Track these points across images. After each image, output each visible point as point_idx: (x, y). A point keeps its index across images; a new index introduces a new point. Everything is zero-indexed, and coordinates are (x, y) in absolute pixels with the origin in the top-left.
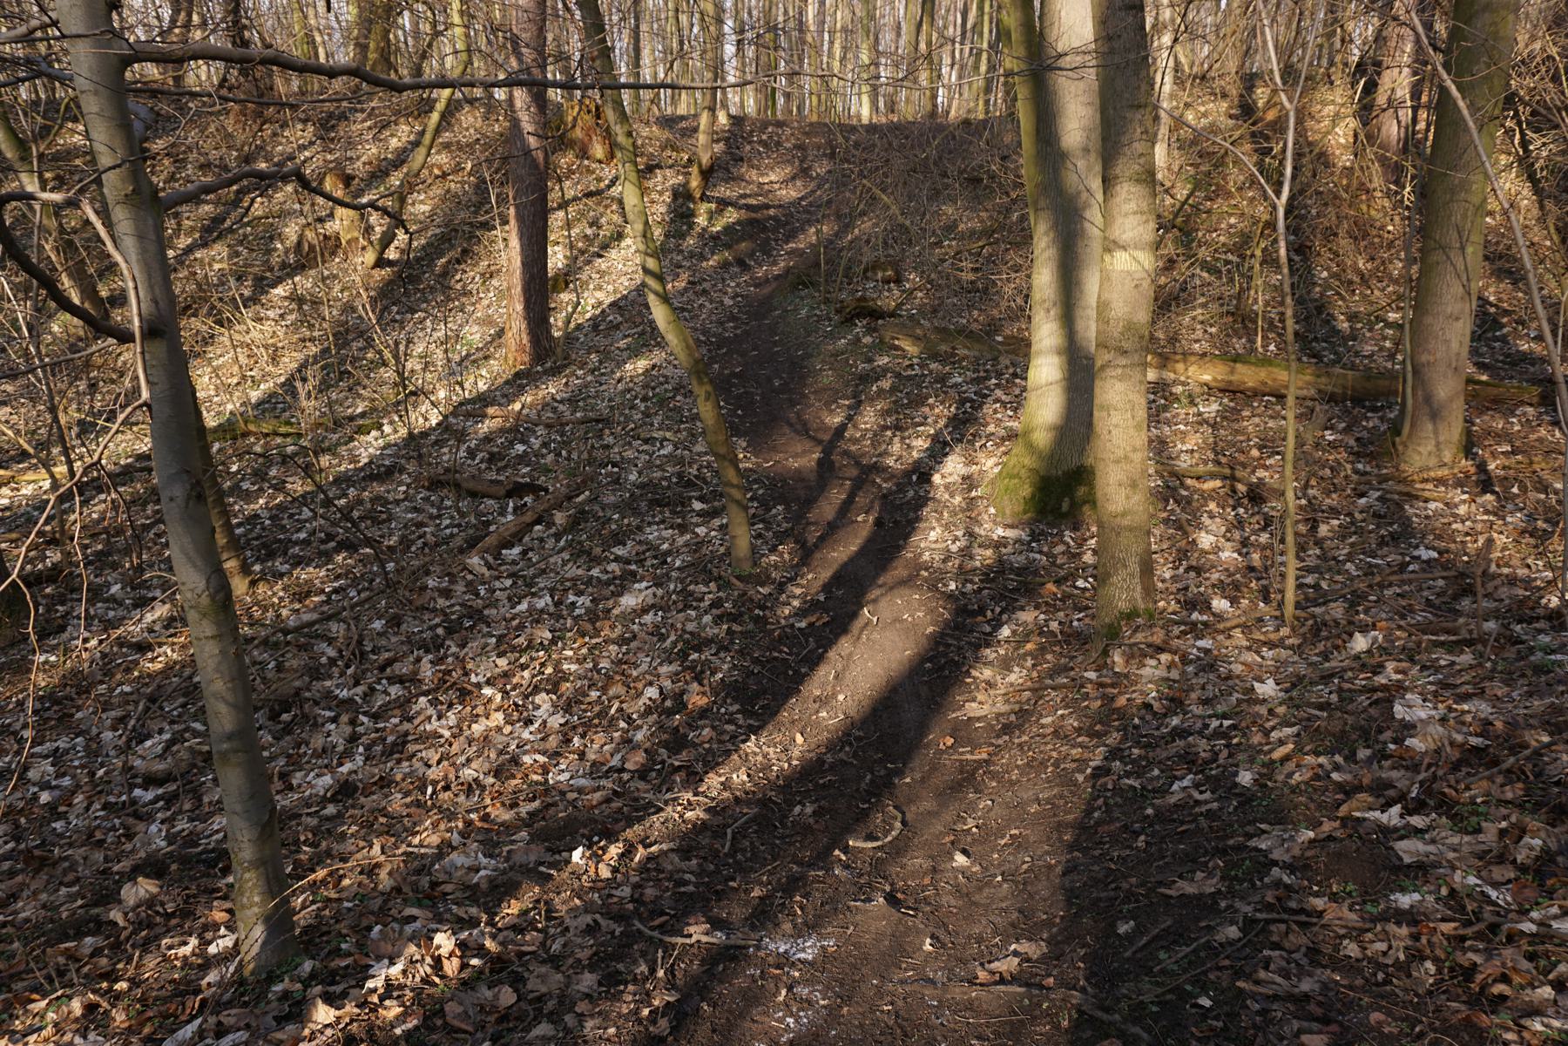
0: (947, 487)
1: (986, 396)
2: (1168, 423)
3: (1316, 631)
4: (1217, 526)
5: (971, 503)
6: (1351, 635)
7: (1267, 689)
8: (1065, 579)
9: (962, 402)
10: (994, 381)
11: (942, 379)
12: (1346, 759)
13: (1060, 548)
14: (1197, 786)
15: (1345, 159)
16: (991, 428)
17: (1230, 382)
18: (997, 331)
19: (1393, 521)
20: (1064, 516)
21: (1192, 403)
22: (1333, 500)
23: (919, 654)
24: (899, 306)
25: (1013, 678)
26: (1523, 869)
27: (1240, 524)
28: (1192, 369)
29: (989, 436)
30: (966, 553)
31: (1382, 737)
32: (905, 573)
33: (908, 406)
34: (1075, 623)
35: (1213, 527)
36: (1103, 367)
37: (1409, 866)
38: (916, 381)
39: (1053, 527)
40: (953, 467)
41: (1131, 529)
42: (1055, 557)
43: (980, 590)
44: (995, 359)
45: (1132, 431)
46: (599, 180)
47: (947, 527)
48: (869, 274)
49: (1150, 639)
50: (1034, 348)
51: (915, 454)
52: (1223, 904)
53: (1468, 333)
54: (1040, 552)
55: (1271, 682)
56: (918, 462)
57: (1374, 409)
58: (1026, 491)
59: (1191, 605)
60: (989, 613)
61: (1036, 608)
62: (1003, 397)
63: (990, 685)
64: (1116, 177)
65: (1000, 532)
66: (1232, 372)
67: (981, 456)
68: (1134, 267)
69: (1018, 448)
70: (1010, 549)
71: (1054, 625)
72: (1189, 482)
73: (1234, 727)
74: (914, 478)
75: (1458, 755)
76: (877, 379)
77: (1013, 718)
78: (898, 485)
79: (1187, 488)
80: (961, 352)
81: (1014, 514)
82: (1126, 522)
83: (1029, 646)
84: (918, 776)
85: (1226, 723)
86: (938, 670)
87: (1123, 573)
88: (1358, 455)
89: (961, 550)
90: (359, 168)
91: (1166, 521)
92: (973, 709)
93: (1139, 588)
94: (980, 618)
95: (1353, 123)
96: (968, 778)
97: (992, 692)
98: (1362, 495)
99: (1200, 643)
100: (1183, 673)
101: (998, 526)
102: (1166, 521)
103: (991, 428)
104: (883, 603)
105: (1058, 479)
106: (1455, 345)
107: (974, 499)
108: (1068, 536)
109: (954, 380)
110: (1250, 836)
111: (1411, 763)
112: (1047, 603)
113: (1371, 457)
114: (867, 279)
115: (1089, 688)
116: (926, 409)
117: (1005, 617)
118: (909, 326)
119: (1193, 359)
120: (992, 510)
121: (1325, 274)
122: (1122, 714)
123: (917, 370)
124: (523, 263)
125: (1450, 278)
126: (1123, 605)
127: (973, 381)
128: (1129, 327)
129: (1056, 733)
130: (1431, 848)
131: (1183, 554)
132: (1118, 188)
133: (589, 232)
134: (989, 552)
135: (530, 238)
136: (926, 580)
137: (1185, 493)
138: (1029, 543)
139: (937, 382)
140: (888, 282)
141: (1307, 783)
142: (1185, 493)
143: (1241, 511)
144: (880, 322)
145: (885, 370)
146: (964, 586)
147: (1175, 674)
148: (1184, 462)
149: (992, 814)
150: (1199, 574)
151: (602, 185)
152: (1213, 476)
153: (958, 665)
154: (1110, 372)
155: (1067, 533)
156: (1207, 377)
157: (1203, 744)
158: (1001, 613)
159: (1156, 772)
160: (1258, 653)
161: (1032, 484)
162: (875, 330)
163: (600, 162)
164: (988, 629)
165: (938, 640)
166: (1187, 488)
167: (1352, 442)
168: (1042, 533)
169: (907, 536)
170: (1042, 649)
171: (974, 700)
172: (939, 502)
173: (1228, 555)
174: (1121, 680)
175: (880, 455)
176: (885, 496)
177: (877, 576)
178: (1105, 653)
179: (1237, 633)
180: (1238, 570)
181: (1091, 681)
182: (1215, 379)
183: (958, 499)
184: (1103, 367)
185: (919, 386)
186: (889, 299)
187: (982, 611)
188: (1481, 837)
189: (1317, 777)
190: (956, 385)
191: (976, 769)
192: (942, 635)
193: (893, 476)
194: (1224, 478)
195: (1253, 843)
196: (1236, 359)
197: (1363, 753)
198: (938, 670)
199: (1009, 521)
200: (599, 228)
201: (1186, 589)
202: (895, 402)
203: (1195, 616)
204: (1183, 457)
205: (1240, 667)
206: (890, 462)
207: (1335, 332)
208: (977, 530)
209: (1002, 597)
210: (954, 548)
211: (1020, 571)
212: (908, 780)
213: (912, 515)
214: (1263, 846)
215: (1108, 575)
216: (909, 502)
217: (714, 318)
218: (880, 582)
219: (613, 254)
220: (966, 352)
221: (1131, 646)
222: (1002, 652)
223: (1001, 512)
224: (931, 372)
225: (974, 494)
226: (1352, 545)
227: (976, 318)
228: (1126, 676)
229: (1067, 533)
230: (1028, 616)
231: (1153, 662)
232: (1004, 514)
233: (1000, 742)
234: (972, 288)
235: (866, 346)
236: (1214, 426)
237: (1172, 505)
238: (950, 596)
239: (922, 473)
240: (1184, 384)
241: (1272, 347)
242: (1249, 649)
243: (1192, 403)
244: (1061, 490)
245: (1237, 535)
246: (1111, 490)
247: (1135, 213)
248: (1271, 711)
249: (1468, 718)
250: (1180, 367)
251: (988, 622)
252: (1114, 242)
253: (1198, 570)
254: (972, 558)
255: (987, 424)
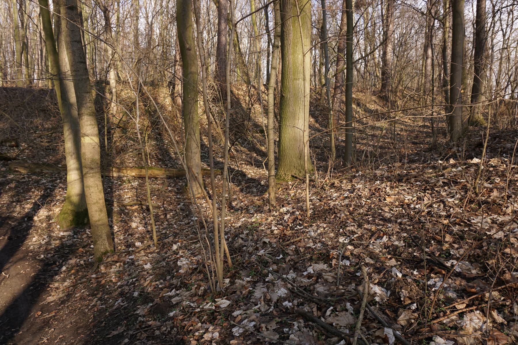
0: (40, 221)
1: (56, 186)
2: (122, 189)
3: (163, 246)
4: (137, 220)
5: (50, 225)
6: (172, 245)
7: (148, 266)
8: (87, 246)
9: (46, 189)
10: (58, 181)
11: (37, 182)
12: (164, 281)
13: (85, 236)
14: (122, 301)
15: (170, 108)
16: (58, 198)
17: (141, 175)
18: (59, 163)
19: (187, 211)
20: (86, 224)
21: (130, 182)
22: (171, 207)
23: (28, 284)
24: (18, 155)
25: (66, 284)
26: (200, 296)
27: (144, 218)
28: (129, 172)
29: (57, 201)
30: (48, 243)
31: (173, 272)
32: (22, 256)
33: (23, 192)
34: (90, 260)
35: (136, 221)
36: (85, 174)
37: (175, 304)
38: (27, 183)
39: (82, 229)
40: (43, 213)
41: (102, 225)
42: (83, 239)
43: (54, 256)
44: (59, 173)
45: (98, 194)
47: (40, 235)
48: (4, 144)
49: (113, 259)
50: (68, 169)
51: (26, 210)
52: (125, 334)
53: (199, 157)
54: (78, 238)
55: (149, 264)
56: (28, 213)
57: (181, 180)
58: (71, 218)
59: (128, 246)
60: (58, 263)
61: (76, 258)
62: (63, 186)
63: (57, 288)
64: (82, 114)
65: (62, 234)
66: (141, 172)
67: (54, 208)
68: (92, 142)
69: (66, 203)
70: (66, 239)
71: (82, 262)
72: (128, 207)
73: (137, 280)
74: (26, 219)
75: (191, 271)
76: (9, 184)
77: (65, 298)
78: (18, 223)
79: (127, 210)
80: (45, 171)
81: (67, 227)
82: (100, 223)
83: (73, 271)
84: (25, 330)
85: (134, 280)
86: (36, 288)
87: (101, 240)
88: (177, 193)
89: (46, 243)
91: (121, 221)
92: (50, 299)
93: (107, 243)
94: (54, 266)
95: (170, 98)
96: (47, 323)
97: (57, 291)
98: (179, 204)
99: (130, 257)
100: (124, 267)
101: (60, 232)
102: (121, 221)
103: (58, 198)
104: (12, 269)
105: (82, 212)
106: (197, 160)
107: (50, 224)
108: (88, 231)
109: (42, 182)
110: (135, 311)
111: (179, 276)
112: (80, 255)
113: (181, 193)
114: (3, 146)
115: (93, 281)
116: (31, 193)
117: (64, 263)
118: (23, 163)
119: (128, 168)
120: (58, 226)
121: (167, 141)
122: (104, 286)
123: (27, 179)
125: (193, 142)
126: (103, 250)
127: (50, 181)
128: (93, 161)
129: (81, 299)
130: (180, 298)
131: (126, 231)
132: (83, 117)
134: (58, 242)
136: (31, 256)
137: (127, 211)
138: (73, 236)
139: (35, 183)
140: (13, 147)
141: (152, 291)
142: (127, 211)
143: (145, 214)
144: (9, 162)
145: (12, 180)
146: (47, 255)
147: (121, 269)
148: (127, 202)
149: (54, 333)
150: (132, 236)
152: (135, 205)
153: (44, 285)
154: (88, 175)
155: (87, 230)
156: (134, 174)
157: (127, 288)
158: (62, 262)
159: (111, 301)
160: (147, 256)
161: (73, 215)
162: (7, 165)
164: (57, 269)
165: (36, 278)
166: (127, 210)
167: (176, 190)
168: (78, 232)
169: (24, 241)
170: (78, 271)
171: (50, 295)
172: (37, 226)
173: (141, 228)
174: (104, 275)
175: (10, 212)
176: (13, 228)
177: (9, 259)
178: (98, 267)
179: (142, 252)
180: (144, 232)
181: (93, 278)
182: (136, 174)
183: (44, 224)
184: (85, 174)
185: (27, 185)
186: (13, 153)
187: (55, 263)
188: (192, 291)
189: (155, 288)
190: (43, 183)
191: (50, 320)
192: (37, 275)
193: (16, 220)
194: (139, 205)
195: (135, 313)
196: (142, 168)
197: (168, 278)
198: (36, 288)
199: (65, 229)
201: (128, 241)
202: (17, 192)
203: (131, 249)
204: (127, 200)
205: (142, 262)
206: (15, 214)
207: (171, 158)
208: (52, 234)
209: (63, 256)
210: (43, 243)
211: (70, 246)
212: (21, 333)
213: (25, 233)
214: (138, 312)
215: (96, 241)
216: (24, 229)
218: (10, 261)
220: (47, 171)
221: (106, 263)
222: (62, 276)
223: (62, 227)
224: (33, 180)
225: (51, 222)
226: (176, 219)
227: (51, 159)
228: (105, 273)
229: (87, 230)
230: (73, 261)
231: (115, 267)
232: (63, 227)
233: (60, 307)
234: (47, 149)
235: (3, 171)
236: (137, 189)
237: (123, 215)
238: (42, 260)
239: (29, 217)
240: (126, 177)
241: (154, 163)
242: (145, 256)
243: (130, 182)
244: (80, 217)
245: (143, 222)
246: (93, 213)
247: (90, 125)
248: (148, 273)
249: (194, 261)
250: (125, 171)
251: (57, 267)
252: (84, 134)
253: (132, 235)
254: (51, 245)
255: (57, 196)
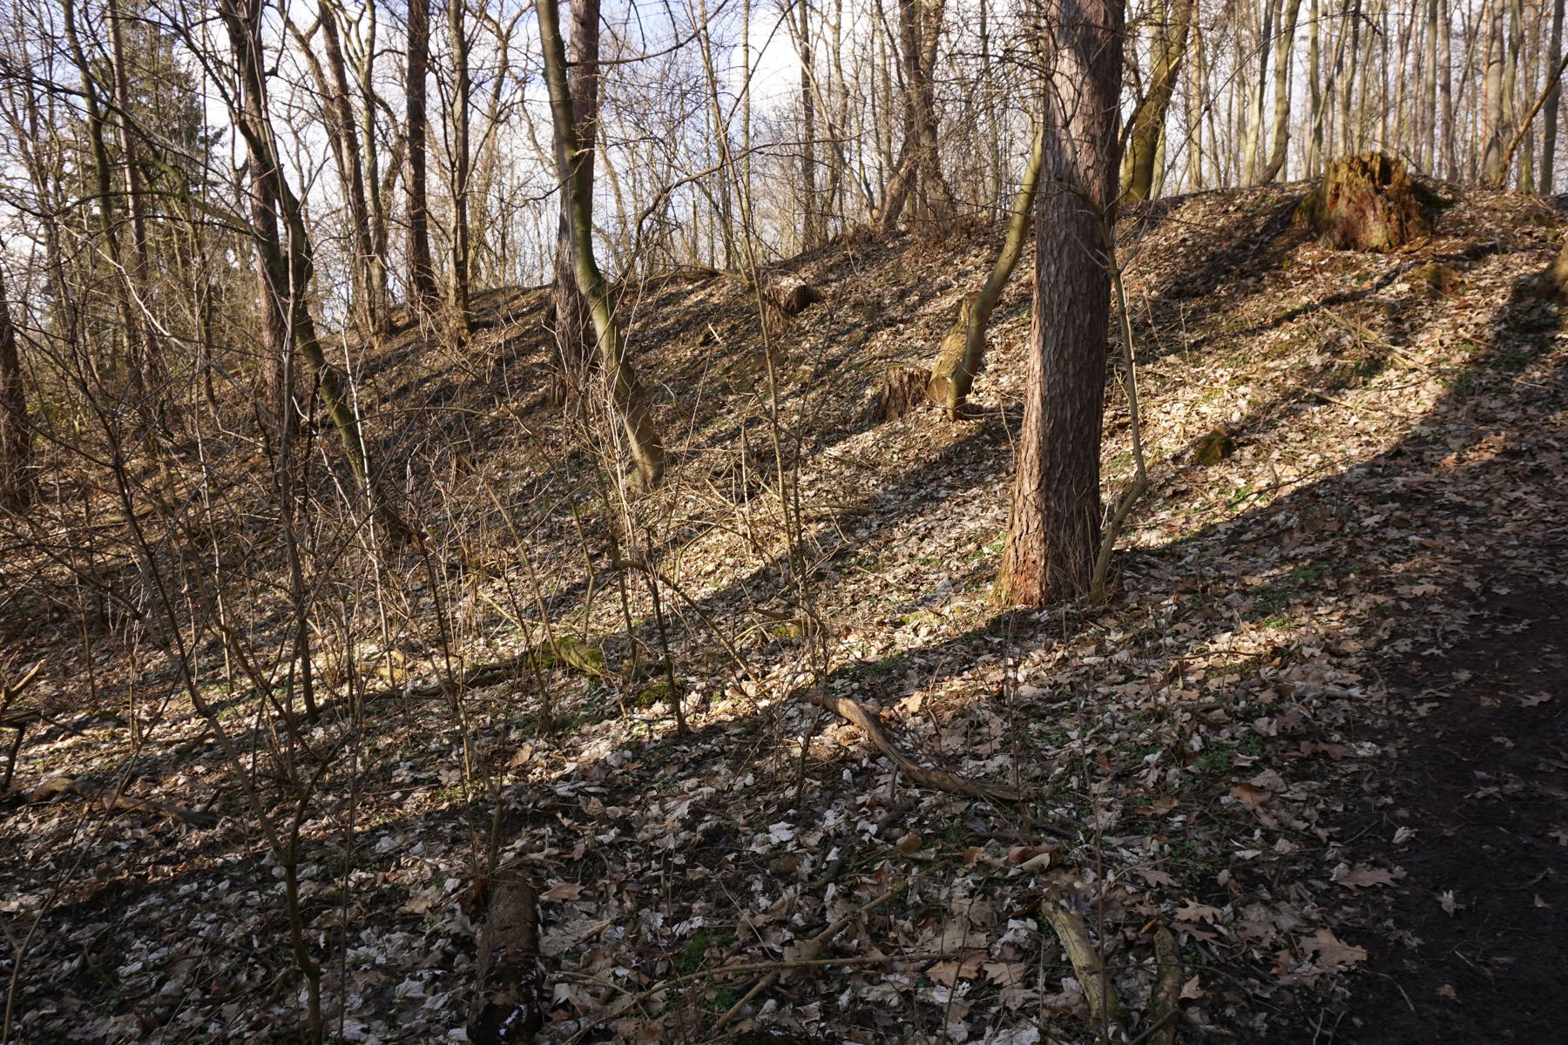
46: (1367, 276)
90: (1494, 175)
124: (1044, 367)
133: (1315, 361)
135: (1060, 349)
151: (1367, 285)
163: (1377, 250)
200: (1337, 353)
217: (1537, 533)
219: (1351, 397)
